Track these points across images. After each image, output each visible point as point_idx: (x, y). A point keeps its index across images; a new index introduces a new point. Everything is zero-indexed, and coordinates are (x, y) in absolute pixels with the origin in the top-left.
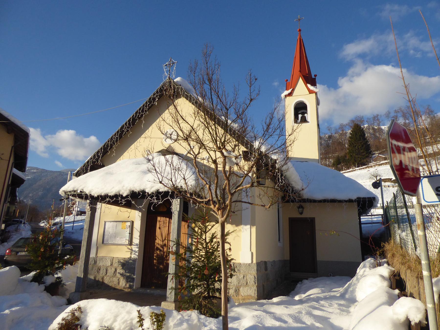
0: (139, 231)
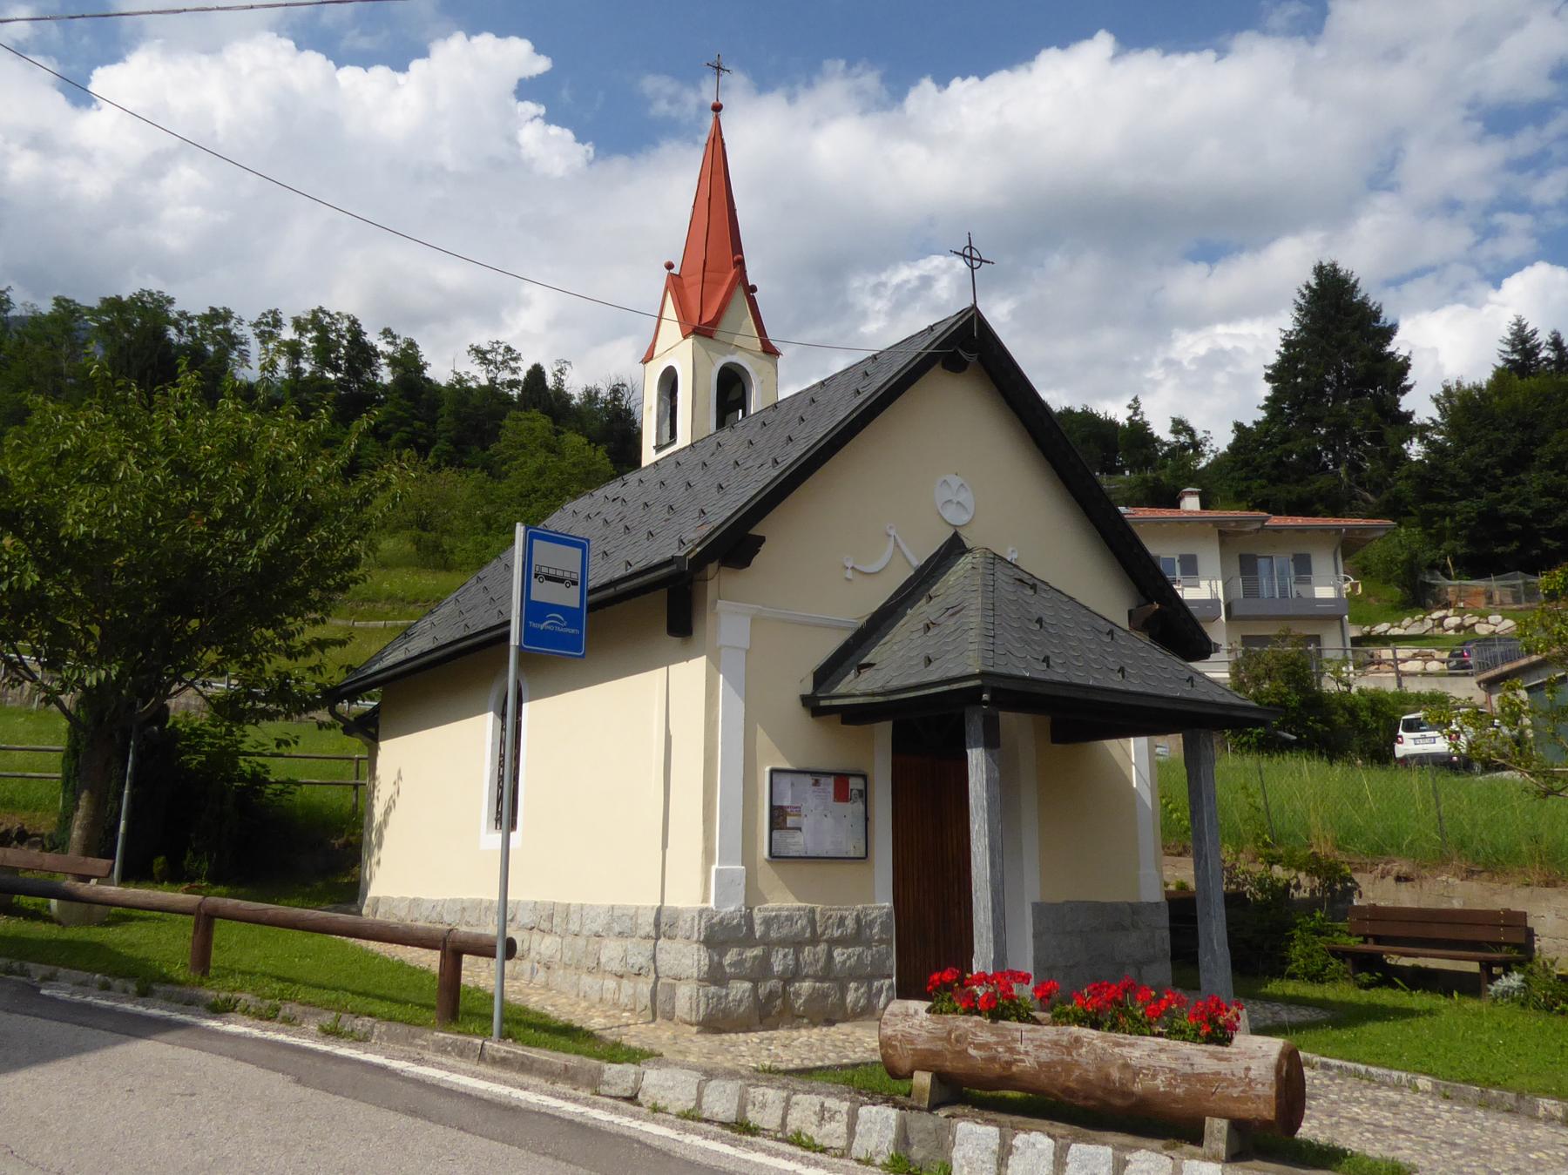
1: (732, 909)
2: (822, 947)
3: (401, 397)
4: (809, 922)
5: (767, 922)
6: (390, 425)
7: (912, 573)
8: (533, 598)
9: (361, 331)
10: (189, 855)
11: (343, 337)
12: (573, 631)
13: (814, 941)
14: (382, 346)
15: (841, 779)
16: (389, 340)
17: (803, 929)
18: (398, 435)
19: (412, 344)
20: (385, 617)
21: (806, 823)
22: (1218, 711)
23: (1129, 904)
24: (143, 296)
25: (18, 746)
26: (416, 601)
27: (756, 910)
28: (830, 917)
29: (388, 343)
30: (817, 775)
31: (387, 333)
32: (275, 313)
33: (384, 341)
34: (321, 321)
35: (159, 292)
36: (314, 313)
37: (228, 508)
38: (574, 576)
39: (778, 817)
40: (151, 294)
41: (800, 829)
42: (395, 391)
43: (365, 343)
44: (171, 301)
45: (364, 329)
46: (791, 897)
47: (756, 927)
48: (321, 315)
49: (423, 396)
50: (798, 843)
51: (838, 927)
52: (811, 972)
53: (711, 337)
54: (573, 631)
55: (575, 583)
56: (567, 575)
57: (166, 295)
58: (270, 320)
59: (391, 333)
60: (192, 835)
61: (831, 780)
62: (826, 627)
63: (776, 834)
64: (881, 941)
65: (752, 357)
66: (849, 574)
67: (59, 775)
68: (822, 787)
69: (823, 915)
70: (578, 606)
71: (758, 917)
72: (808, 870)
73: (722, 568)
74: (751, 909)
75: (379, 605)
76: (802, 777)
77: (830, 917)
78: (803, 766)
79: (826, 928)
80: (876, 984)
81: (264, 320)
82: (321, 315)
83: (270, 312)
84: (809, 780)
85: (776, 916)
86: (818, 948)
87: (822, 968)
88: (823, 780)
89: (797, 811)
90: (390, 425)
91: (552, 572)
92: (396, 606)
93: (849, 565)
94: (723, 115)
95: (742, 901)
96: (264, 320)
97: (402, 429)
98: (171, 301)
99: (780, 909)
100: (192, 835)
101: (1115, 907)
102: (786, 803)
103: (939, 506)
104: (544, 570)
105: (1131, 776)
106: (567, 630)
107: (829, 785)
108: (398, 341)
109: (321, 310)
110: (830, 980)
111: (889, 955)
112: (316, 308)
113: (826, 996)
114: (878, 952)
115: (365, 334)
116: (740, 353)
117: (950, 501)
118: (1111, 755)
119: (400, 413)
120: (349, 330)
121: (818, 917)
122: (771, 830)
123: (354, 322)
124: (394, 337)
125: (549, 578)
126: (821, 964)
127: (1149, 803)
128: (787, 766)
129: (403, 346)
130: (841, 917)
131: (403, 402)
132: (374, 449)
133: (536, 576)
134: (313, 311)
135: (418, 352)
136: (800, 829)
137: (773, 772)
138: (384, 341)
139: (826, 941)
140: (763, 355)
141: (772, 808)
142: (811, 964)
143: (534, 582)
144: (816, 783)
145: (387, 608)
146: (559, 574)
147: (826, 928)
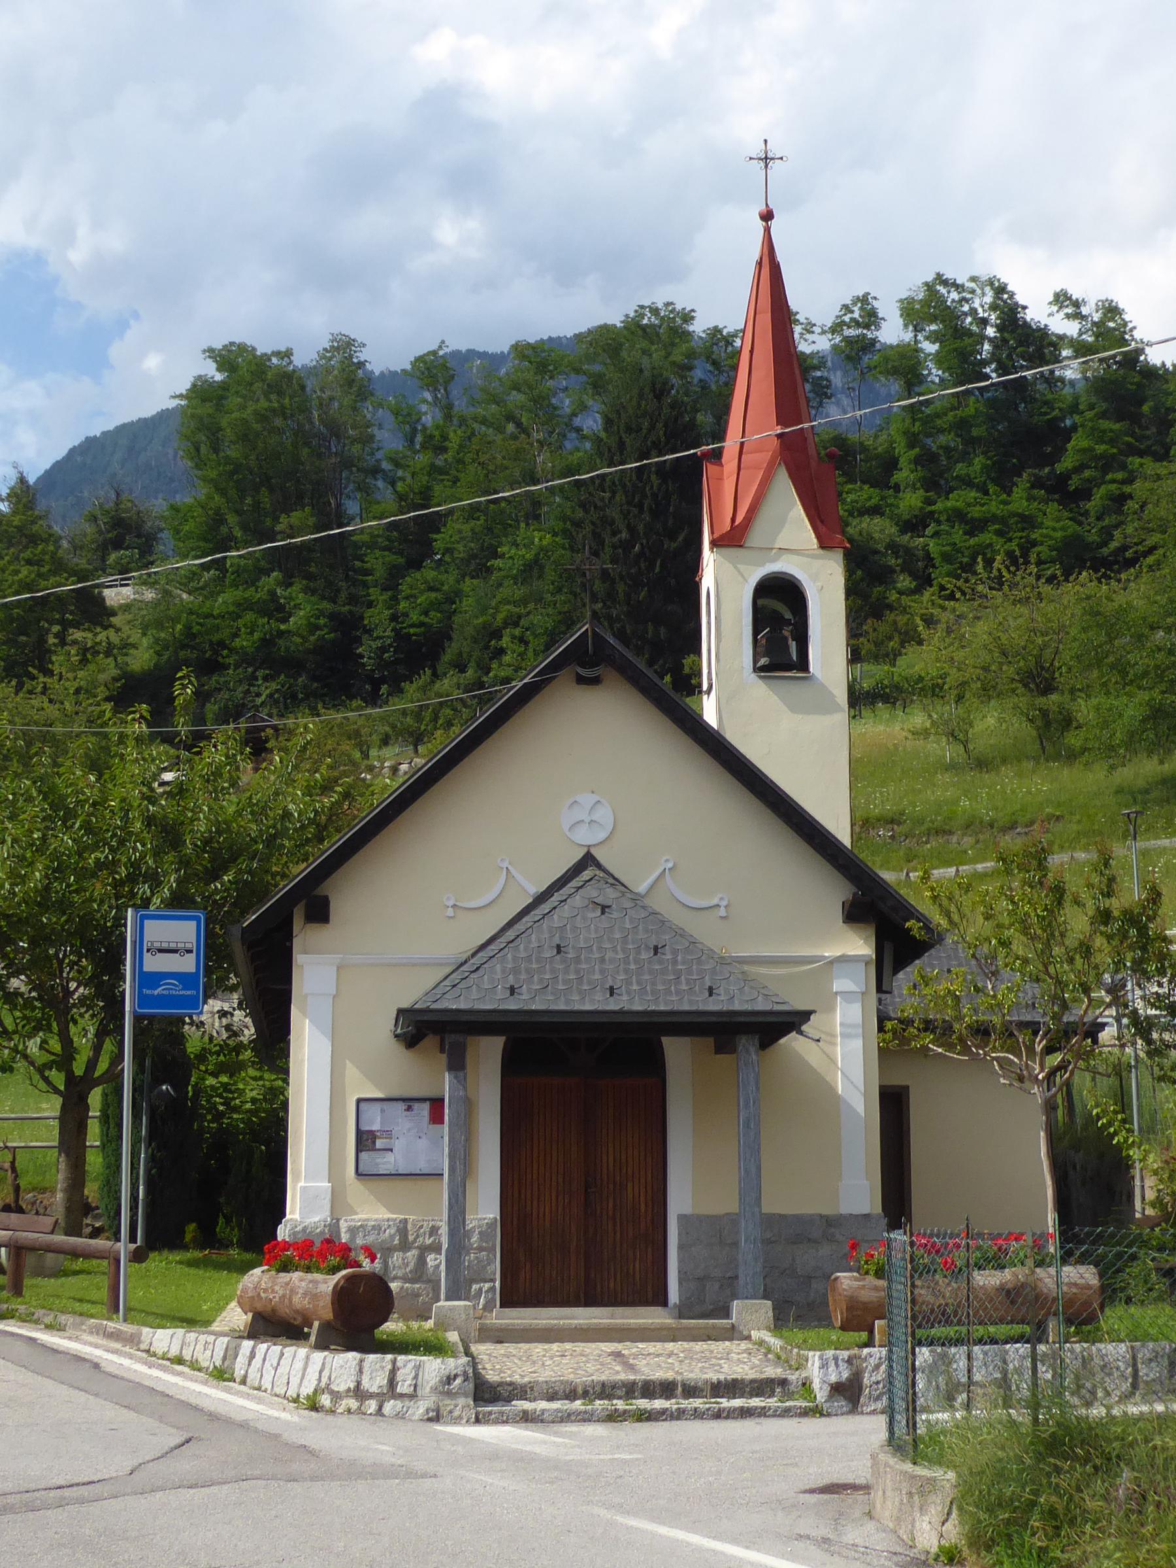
0: (862, 1089)
1: (317, 1219)
2: (412, 1254)
3: (1103, 415)
4: (398, 1230)
5: (353, 1231)
6: (1087, 473)
7: (531, 900)
8: (145, 969)
9: (1016, 304)
10: (221, 1220)
11: (984, 322)
12: (189, 993)
13: (405, 1246)
14: (1061, 325)
15: (436, 1104)
16: (1069, 310)
17: (392, 1237)
18: (1103, 490)
19: (1112, 310)
20: (959, 858)
21: (398, 1145)
22: (714, 1019)
23: (821, 1216)
24: (642, 316)
25: (13, 1116)
26: (1013, 826)
27: (342, 1222)
28: (421, 1227)
29: (1068, 316)
30: (409, 1102)
31: (1061, 299)
32: (864, 300)
33: (1062, 314)
34: (942, 300)
35: (668, 304)
36: (929, 287)
37: (135, 865)
38: (189, 946)
39: (365, 1140)
40: (655, 311)
41: (391, 1150)
42: (1091, 407)
43: (1026, 325)
44: (688, 317)
45: (1020, 299)
46: (383, 1210)
47: (343, 1235)
48: (942, 290)
49: (1146, 408)
50: (387, 1163)
51: (430, 1236)
52: (400, 1274)
53: (741, 546)
54: (189, 993)
55: (189, 951)
56: (180, 945)
57: (679, 307)
58: (856, 315)
59: (1070, 298)
60: (222, 1200)
61: (427, 1106)
62: (427, 965)
63: (364, 1156)
64: (480, 1249)
65: (805, 559)
66: (450, 912)
67: (98, 1143)
68: (415, 1112)
69: (414, 1225)
70: (194, 970)
71: (343, 1226)
72: (383, 1185)
73: (308, 925)
74: (338, 1220)
75: (954, 839)
76: (394, 1104)
77: (421, 1227)
78: (396, 1093)
79: (418, 1236)
80: (474, 1287)
81: (847, 319)
82: (942, 290)
83: (857, 300)
84: (401, 1106)
85: (361, 1226)
86: (409, 1254)
87: (411, 1272)
88: (416, 1106)
89: (388, 1134)
90: (1087, 473)
91: (165, 945)
92: (981, 837)
93: (451, 903)
94: (774, 224)
95: (328, 1213)
96: (847, 319)
97: (1109, 477)
98: (688, 317)
99: (367, 1220)
100: (222, 1200)
101: (799, 1219)
102: (375, 1127)
103: (566, 827)
104: (157, 945)
105: (836, 1083)
106: (181, 993)
107: (424, 1110)
108: (1085, 311)
109: (940, 279)
110: (423, 1282)
111: (490, 1262)
112: (930, 278)
113: (418, 1295)
114: (477, 1258)
115: (1024, 308)
116: (786, 557)
117: (583, 821)
118: (807, 1064)
119: (1101, 448)
120: (994, 307)
121: (409, 1227)
122: (358, 1151)
123: (1001, 289)
124: (1077, 304)
125: (161, 951)
126: (411, 1266)
127: (860, 1109)
128: (380, 1095)
129: (1096, 317)
130: (433, 1227)
131: (1105, 424)
132: (1058, 525)
133: (148, 951)
134: (926, 284)
135: (1125, 324)
136: (391, 1150)
137: (359, 1101)
138: (1062, 314)
139: (418, 1247)
140: (821, 552)
141: (359, 1133)
142: (400, 1267)
143: (147, 956)
144: (409, 1109)
145: (968, 840)
146: (173, 946)
147: (418, 1236)
